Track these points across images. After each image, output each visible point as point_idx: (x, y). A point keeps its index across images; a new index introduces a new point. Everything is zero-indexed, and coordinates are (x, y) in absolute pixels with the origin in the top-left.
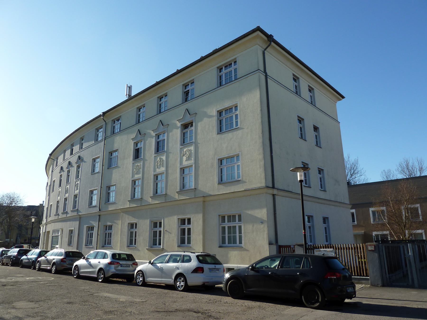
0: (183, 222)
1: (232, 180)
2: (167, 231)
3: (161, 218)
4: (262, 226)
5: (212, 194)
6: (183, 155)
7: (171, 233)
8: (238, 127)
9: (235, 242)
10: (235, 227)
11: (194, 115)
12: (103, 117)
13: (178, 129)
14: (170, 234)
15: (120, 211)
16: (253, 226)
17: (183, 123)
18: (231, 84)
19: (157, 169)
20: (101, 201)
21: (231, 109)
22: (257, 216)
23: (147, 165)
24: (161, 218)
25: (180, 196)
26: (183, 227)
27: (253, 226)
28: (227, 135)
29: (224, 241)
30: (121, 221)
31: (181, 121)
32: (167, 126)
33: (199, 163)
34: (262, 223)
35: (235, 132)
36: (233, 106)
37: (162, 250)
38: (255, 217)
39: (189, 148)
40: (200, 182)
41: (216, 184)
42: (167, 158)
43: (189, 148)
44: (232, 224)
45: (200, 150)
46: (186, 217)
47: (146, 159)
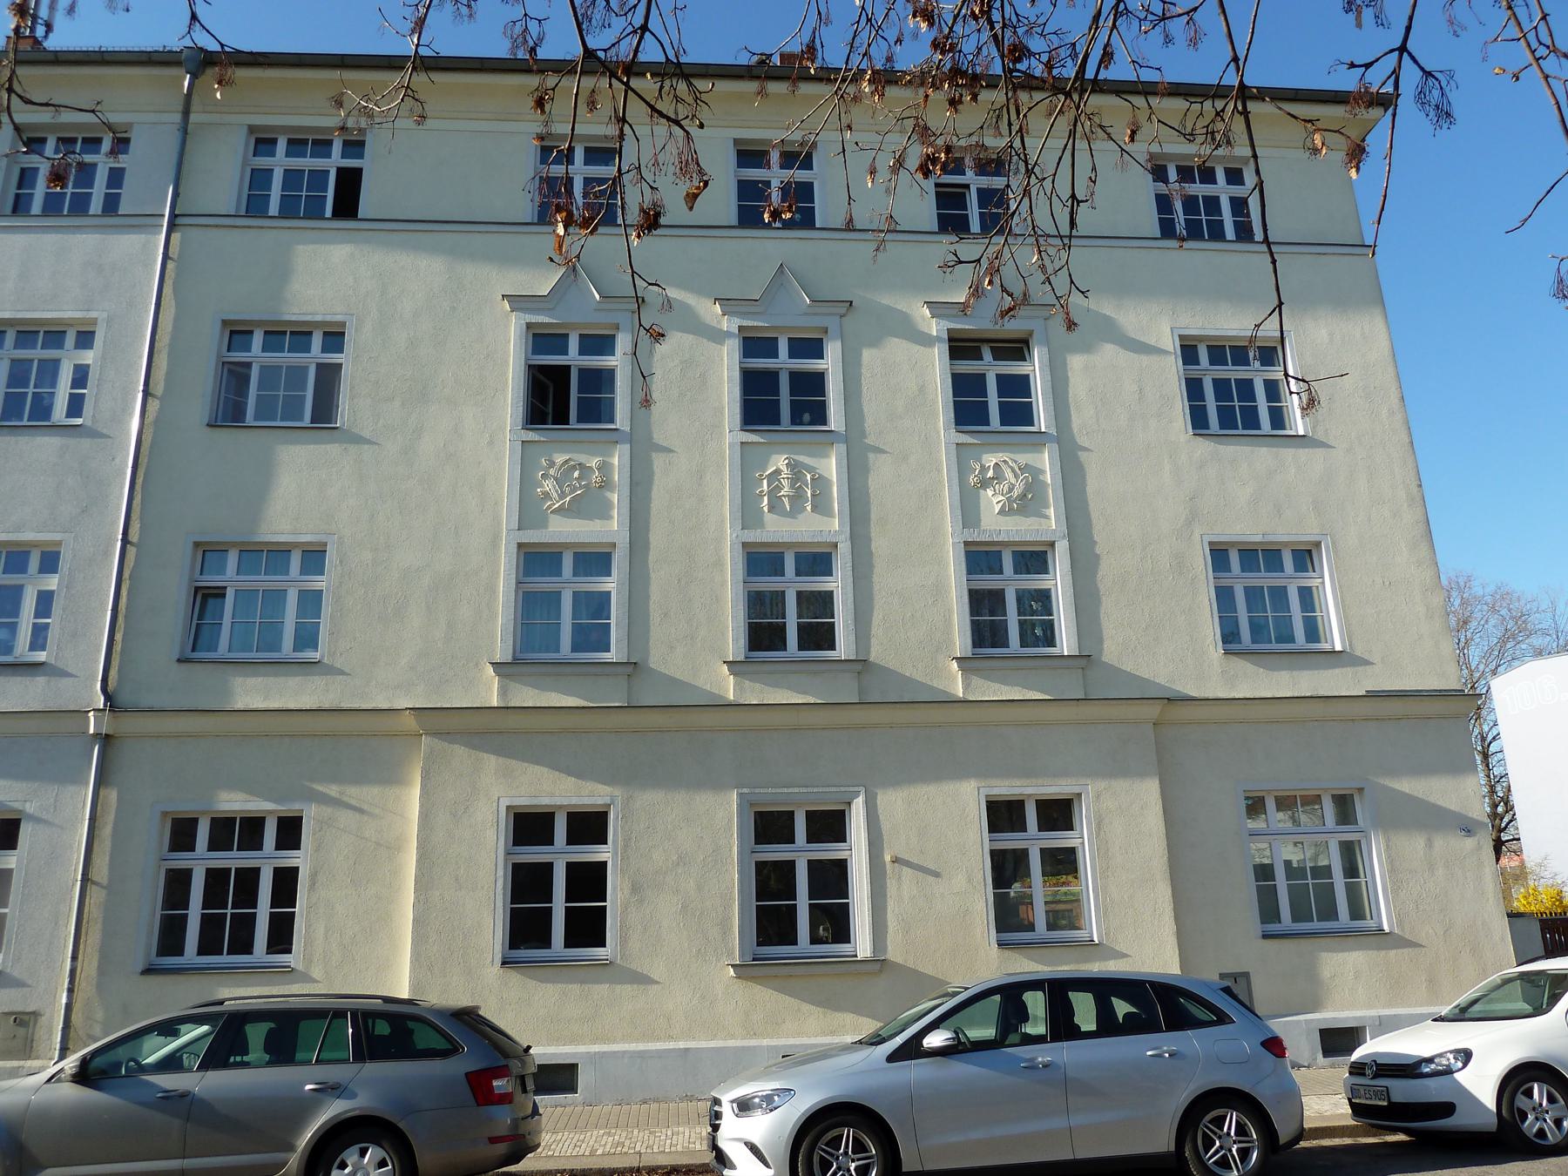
0: (1003, 815)
1: (232, 655)
2: (908, 864)
3: (852, 789)
4: (1469, 843)
5: (1194, 694)
6: (984, 483)
7: (937, 875)
8: (79, 421)
9: (1330, 913)
10: (249, 879)
11: (842, 309)
12: (194, 76)
13: (721, 343)
14: (931, 879)
15: (410, 722)
16: (1429, 844)
17: (971, 327)
18: (1236, 251)
19: (769, 518)
20: (119, 637)
21: (303, 338)
22: (1441, 803)
23: (666, 478)
24: (852, 789)
25: (976, 681)
26: (181, 861)
27: (1429, 844)
28: (1247, 449)
29: (171, 938)
30: (416, 791)
31: (743, 309)
32: (843, 311)
33: (1096, 538)
34: (1469, 831)
35: (9, 438)
36: (70, 323)
37: (881, 971)
38: (1434, 806)
39: (582, 458)
40: (877, 628)
41: (1212, 648)
42: (856, 472)
43: (582, 458)
44: (234, 860)
45: (1092, 486)
46: (1031, 788)
47: (658, 437)
